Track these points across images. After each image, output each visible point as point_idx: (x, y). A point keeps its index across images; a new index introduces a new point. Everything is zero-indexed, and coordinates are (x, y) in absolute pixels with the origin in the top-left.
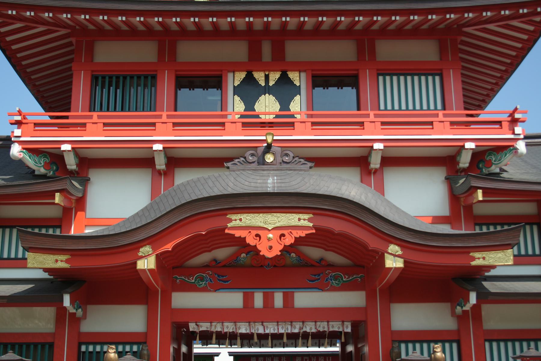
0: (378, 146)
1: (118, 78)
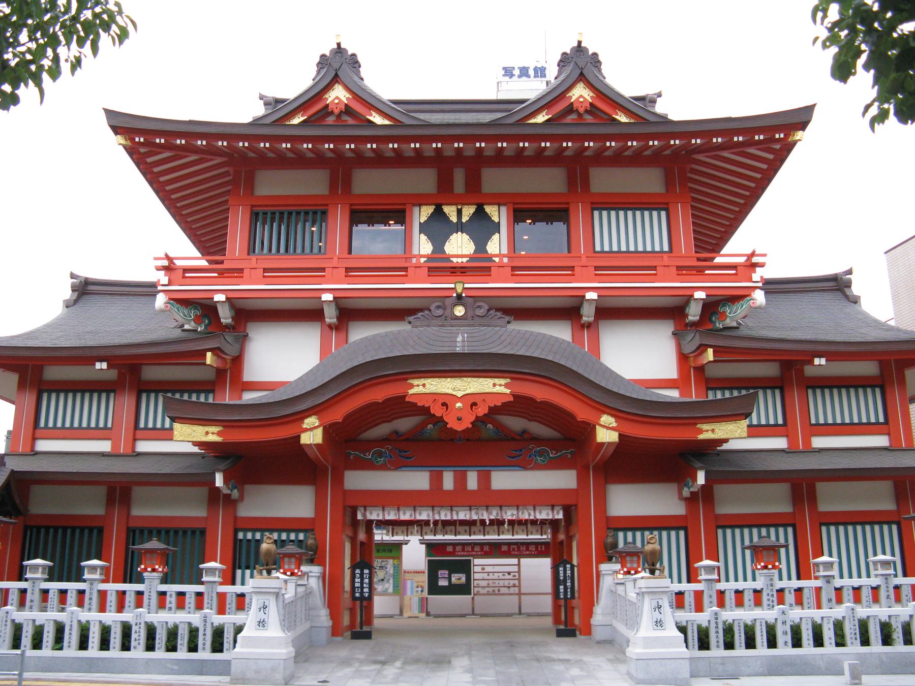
0: (591, 295)
1: (282, 214)
